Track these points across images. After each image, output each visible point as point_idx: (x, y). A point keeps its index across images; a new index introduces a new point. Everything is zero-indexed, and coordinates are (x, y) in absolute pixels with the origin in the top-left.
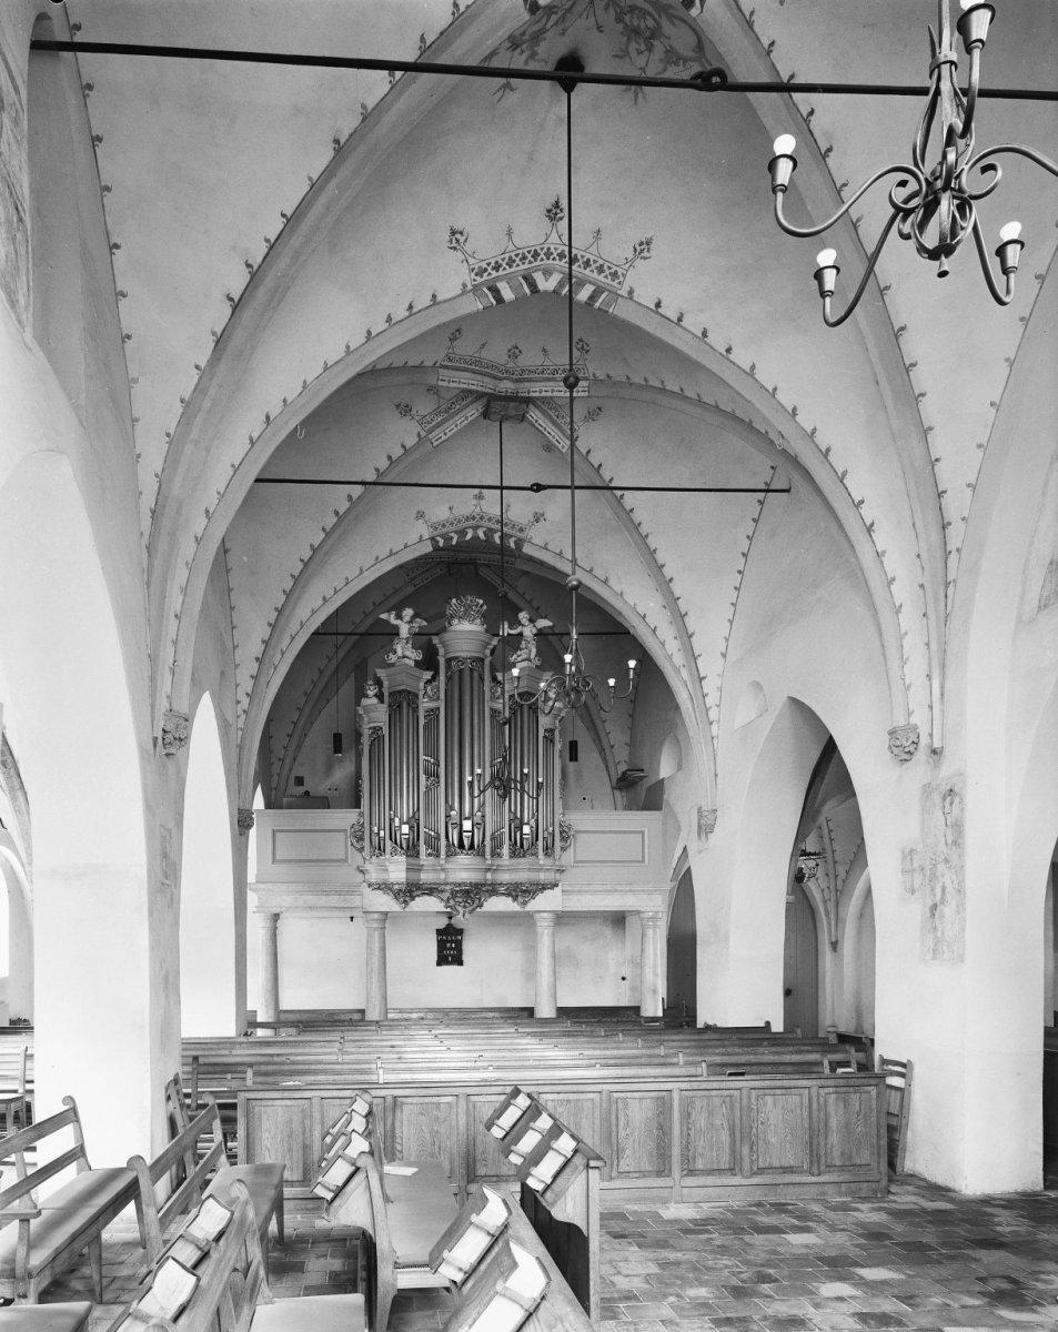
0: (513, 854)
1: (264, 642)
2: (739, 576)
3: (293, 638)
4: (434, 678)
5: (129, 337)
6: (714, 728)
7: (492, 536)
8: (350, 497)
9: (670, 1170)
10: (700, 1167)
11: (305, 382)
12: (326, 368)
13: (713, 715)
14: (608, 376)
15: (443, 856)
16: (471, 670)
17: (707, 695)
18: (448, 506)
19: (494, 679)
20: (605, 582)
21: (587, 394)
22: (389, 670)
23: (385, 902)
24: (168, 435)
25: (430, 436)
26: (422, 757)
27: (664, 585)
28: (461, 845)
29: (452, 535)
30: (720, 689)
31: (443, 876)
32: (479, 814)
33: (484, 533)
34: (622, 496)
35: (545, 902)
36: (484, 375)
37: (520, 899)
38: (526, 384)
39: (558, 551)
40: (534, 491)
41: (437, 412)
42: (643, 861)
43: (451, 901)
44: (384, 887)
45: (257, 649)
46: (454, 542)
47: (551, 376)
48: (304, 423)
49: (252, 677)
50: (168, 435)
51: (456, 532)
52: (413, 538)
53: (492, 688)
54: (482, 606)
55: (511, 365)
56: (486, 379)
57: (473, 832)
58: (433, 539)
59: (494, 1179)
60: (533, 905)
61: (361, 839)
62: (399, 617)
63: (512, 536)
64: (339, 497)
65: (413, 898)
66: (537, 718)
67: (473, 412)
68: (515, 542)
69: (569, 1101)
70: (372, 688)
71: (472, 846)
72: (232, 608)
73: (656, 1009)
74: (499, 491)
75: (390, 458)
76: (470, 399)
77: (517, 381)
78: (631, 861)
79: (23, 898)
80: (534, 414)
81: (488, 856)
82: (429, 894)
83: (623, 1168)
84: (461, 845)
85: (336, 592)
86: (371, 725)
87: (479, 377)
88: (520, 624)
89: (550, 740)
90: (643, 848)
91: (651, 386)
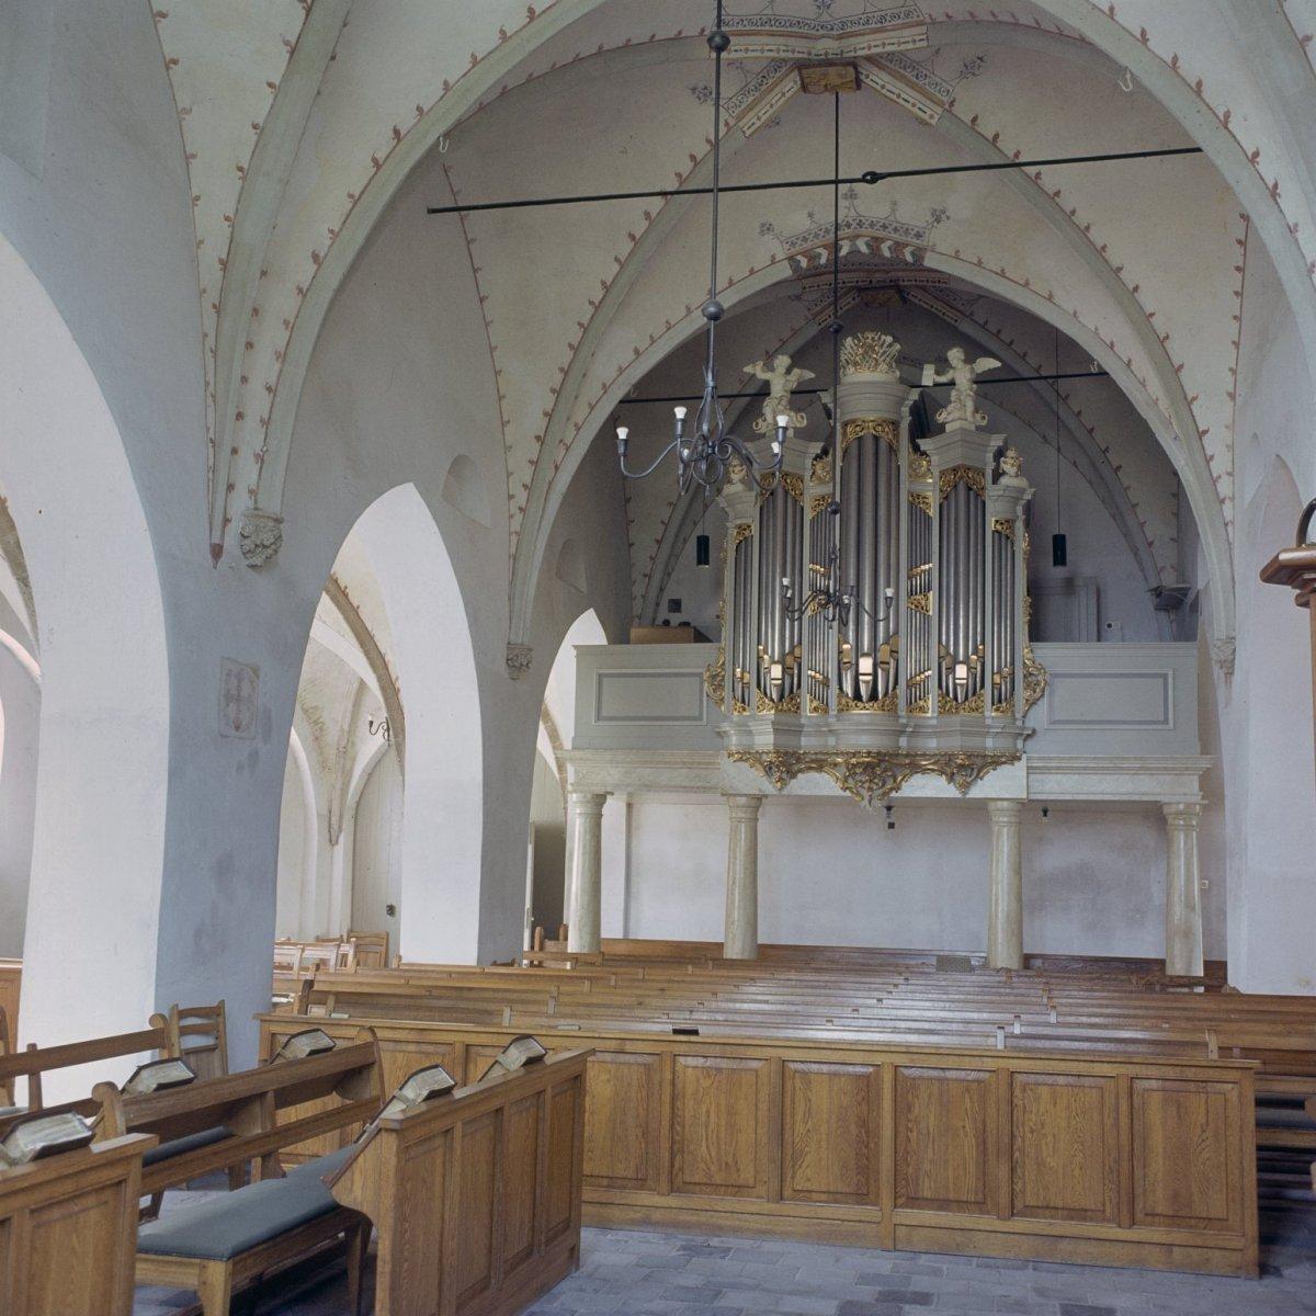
0: (943, 709)
1: (546, 414)
2: (1240, 275)
3: (592, 408)
4: (825, 452)
5: (175, 62)
6: (1227, 508)
7: (878, 248)
8: (647, 215)
9: (878, 1195)
10: (927, 1194)
11: (446, 83)
12: (475, 62)
13: (1224, 488)
14: (947, 15)
15: (833, 711)
16: (876, 439)
17: (1212, 457)
18: (806, 212)
19: (916, 448)
20: (1050, 298)
21: (924, 44)
22: (757, 443)
23: (753, 780)
24: (240, 169)
25: (741, 124)
26: (808, 566)
27: (1126, 297)
28: (857, 696)
29: (820, 250)
30: (1231, 448)
31: (832, 741)
32: (887, 648)
33: (868, 245)
34: (1038, 175)
35: (1000, 785)
36: (789, 35)
37: (958, 778)
38: (853, 40)
39: (975, 260)
40: (867, 182)
41: (744, 91)
42: (1166, 721)
43: (850, 780)
44: (748, 755)
45: (537, 424)
46: (823, 261)
47: (879, 25)
48: (447, 135)
49: (531, 462)
50: (240, 169)
51: (825, 247)
52: (761, 260)
53: (910, 466)
54: (890, 345)
55: (825, 17)
56: (792, 41)
57: (875, 675)
58: (791, 259)
59: (605, 1182)
60: (979, 791)
61: (720, 686)
62: (770, 368)
63: (907, 245)
64: (633, 215)
65: (793, 775)
66: (984, 503)
67: (791, 84)
68: (913, 254)
69: (719, 1070)
70: (737, 469)
71: (873, 696)
72: (497, 373)
73: (1189, 964)
74: (833, 186)
75: (693, 157)
76: (783, 70)
77: (840, 37)
78: (1068, 722)
79: (297, 767)
80: (877, 78)
81: (902, 710)
82: (820, 769)
83: (800, 1184)
84: (857, 696)
85: (653, 341)
86: (739, 522)
87: (781, 40)
88: (773, 370)
89: (1004, 538)
90: (644, 675)
91: (1001, 22)
